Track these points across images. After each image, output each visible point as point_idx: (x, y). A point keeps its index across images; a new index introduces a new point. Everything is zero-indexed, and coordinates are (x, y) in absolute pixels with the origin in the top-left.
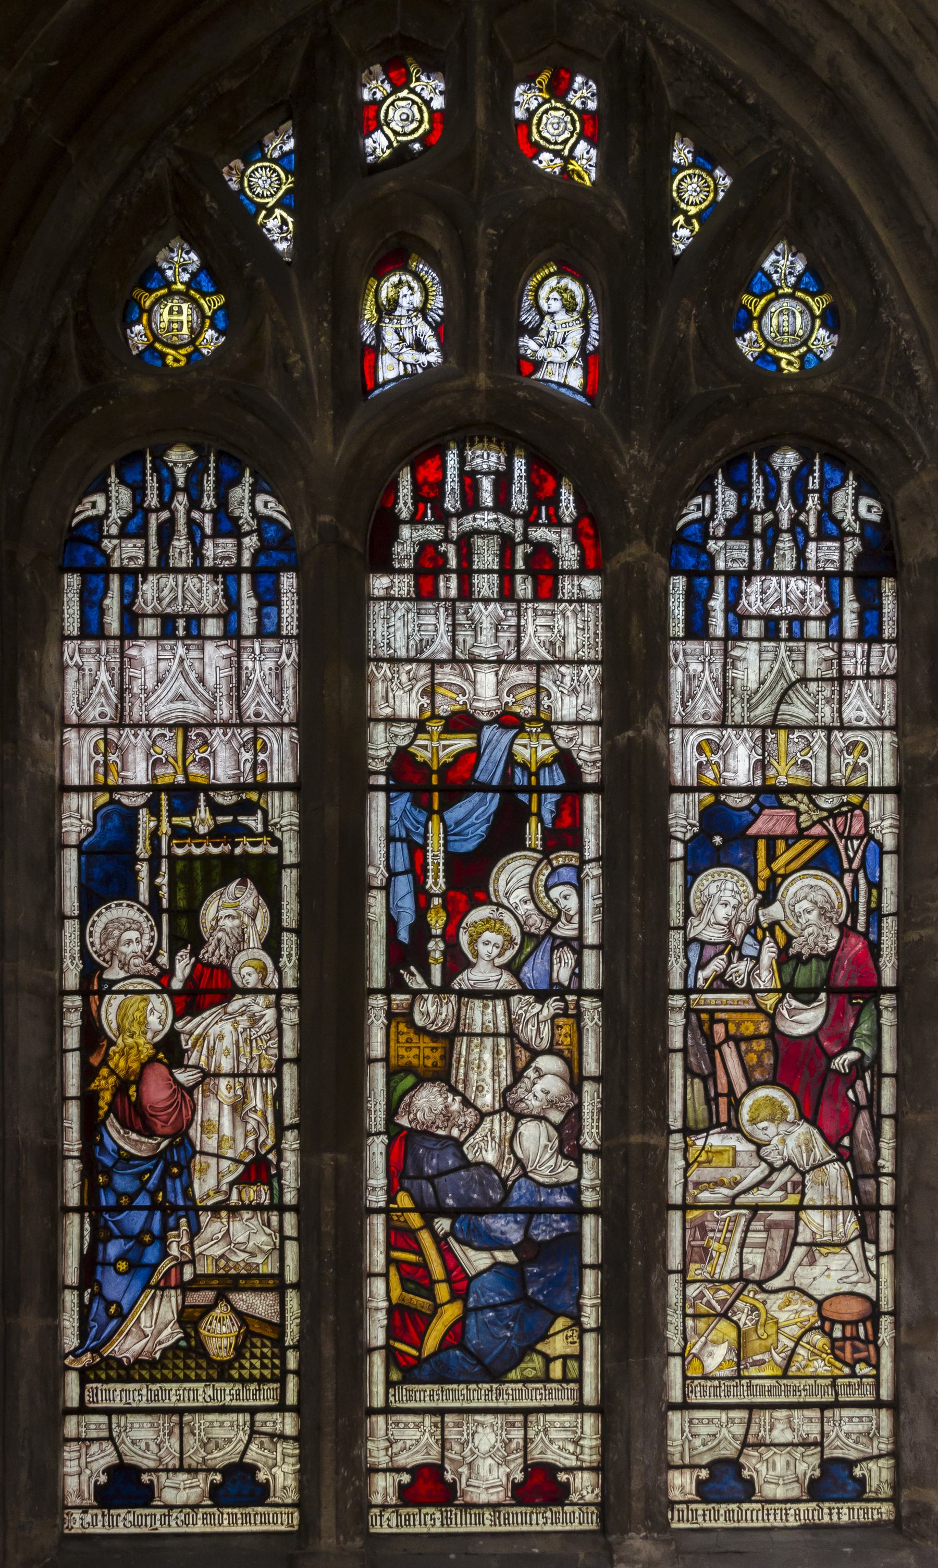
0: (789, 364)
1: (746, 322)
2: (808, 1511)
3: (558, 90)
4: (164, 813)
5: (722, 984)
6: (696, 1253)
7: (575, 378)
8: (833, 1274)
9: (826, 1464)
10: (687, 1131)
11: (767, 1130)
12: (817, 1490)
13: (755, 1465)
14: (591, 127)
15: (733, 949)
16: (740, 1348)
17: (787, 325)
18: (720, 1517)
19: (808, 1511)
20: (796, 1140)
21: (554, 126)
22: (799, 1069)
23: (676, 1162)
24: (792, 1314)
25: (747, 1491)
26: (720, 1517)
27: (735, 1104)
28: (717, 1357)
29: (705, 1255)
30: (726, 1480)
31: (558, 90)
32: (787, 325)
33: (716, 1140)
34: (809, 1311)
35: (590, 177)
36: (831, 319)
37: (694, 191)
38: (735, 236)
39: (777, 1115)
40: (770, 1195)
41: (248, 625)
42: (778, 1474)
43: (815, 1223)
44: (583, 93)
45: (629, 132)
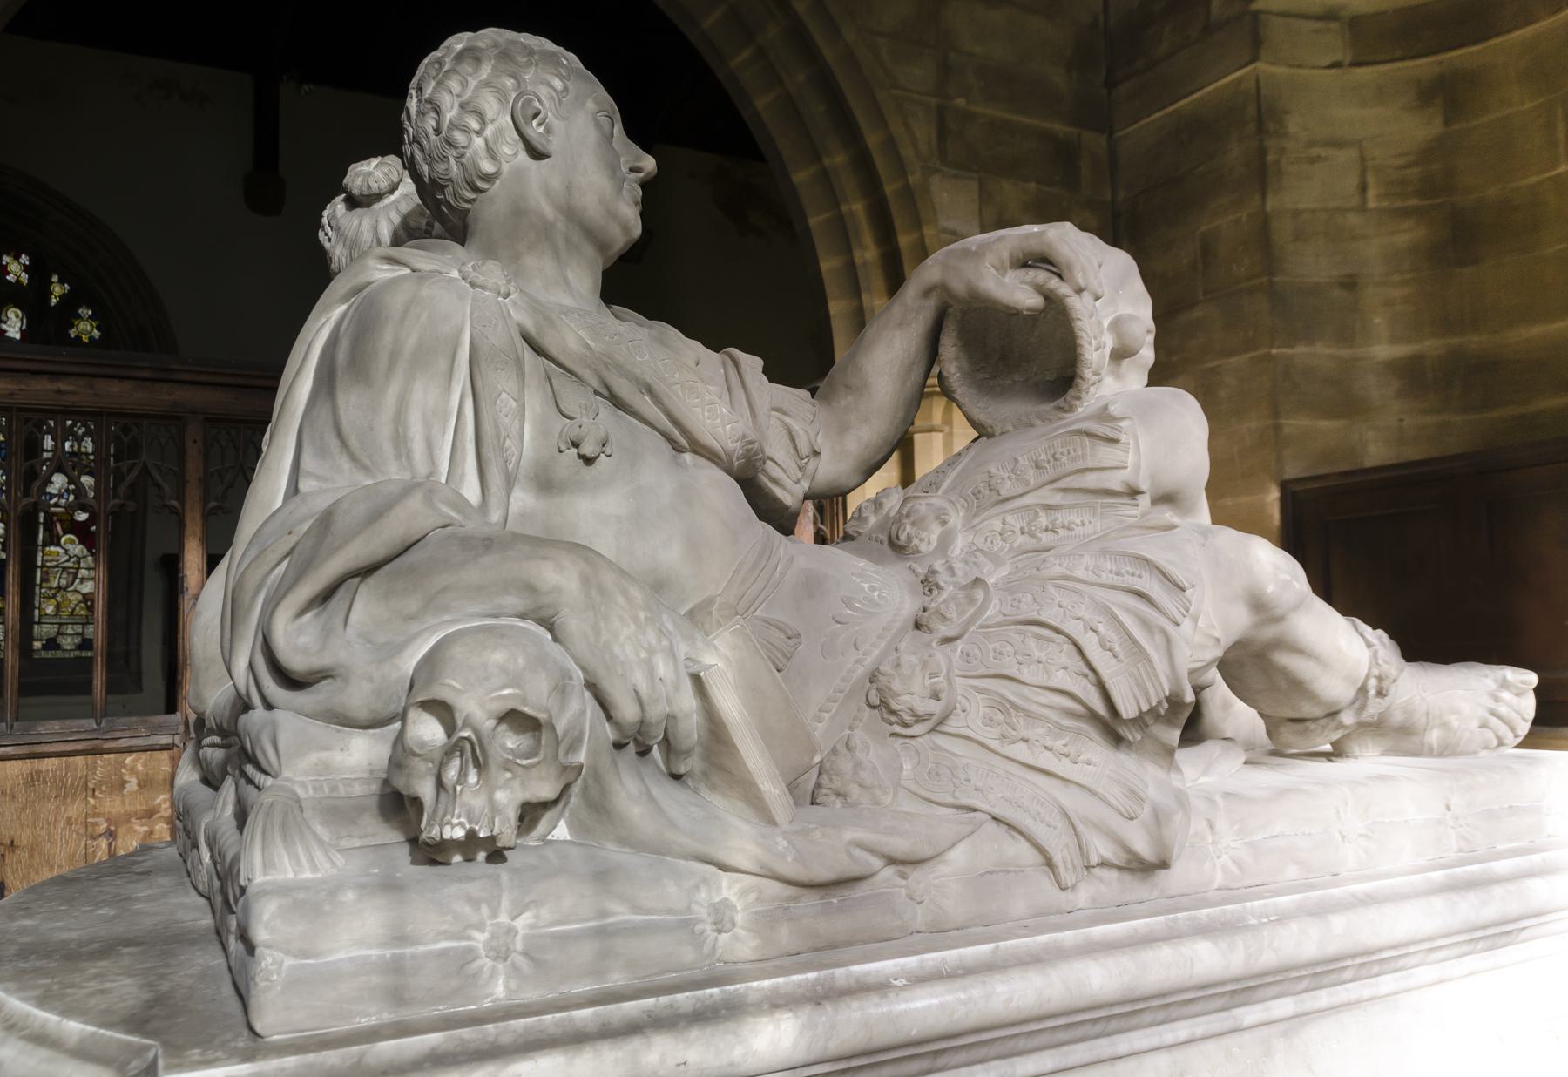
0: (85, 339)
1: (72, 326)
2: (77, 653)
3: (17, 258)
4: (117, 393)
5: (56, 505)
6: (45, 579)
7: (18, 336)
8: (87, 588)
9: (84, 640)
10: (44, 545)
11: (70, 547)
12: (80, 647)
13: (61, 640)
14: (26, 269)
15: (60, 496)
16: (58, 607)
17: (85, 328)
18: (49, 655)
19: (77, 653)
20: (78, 549)
21: (15, 267)
22: (83, 534)
23: (40, 555)
24: (74, 598)
25: (58, 647)
26: (49, 655)
27: (59, 538)
28: (50, 610)
29: (47, 580)
30: (52, 644)
31: (17, 258)
32: (85, 328)
33: (53, 548)
34: (80, 597)
35: (25, 282)
36: (98, 328)
37: (57, 290)
38: (69, 305)
39: (72, 542)
40: (70, 564)
41: (1494, 721)
42: (67, 643)
43: (83, 573)
44: (24, 259)
45: (38, 272)
